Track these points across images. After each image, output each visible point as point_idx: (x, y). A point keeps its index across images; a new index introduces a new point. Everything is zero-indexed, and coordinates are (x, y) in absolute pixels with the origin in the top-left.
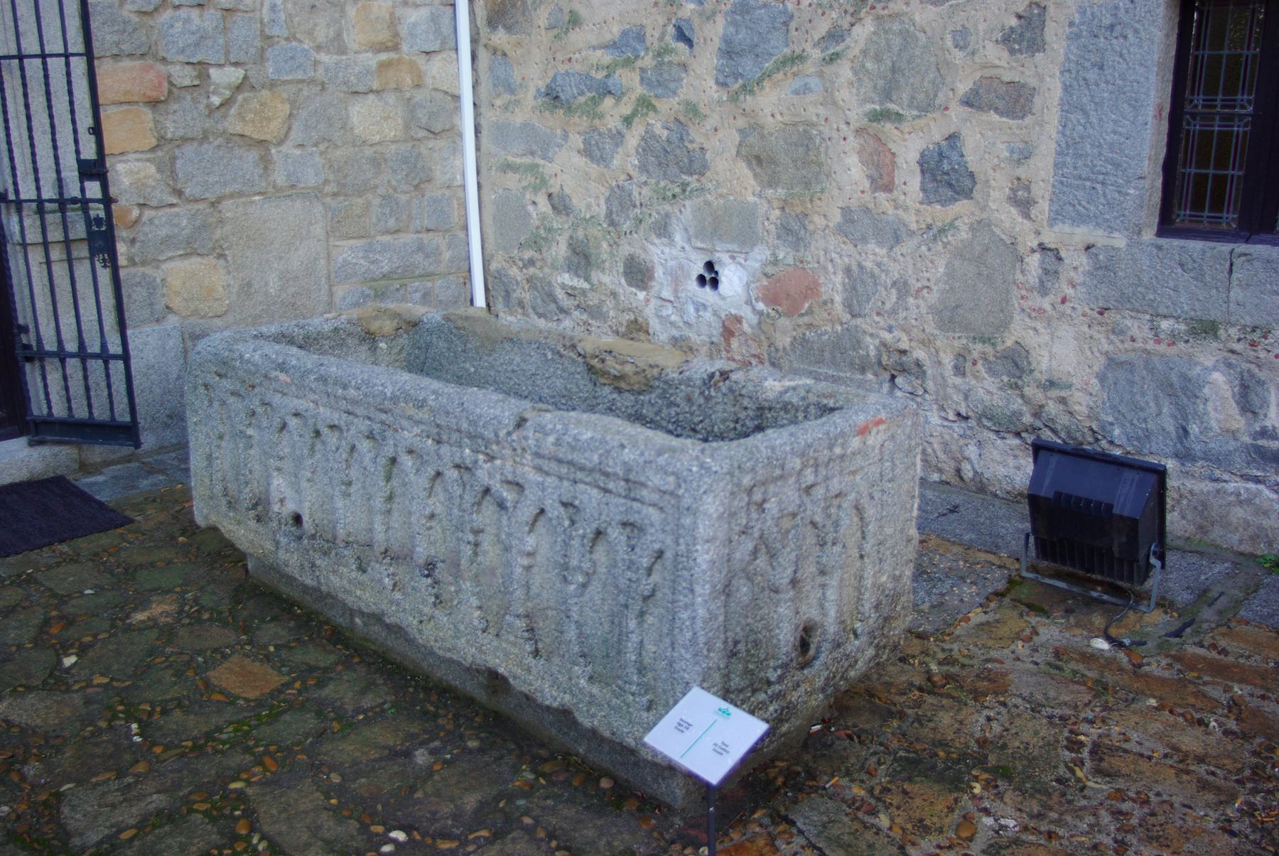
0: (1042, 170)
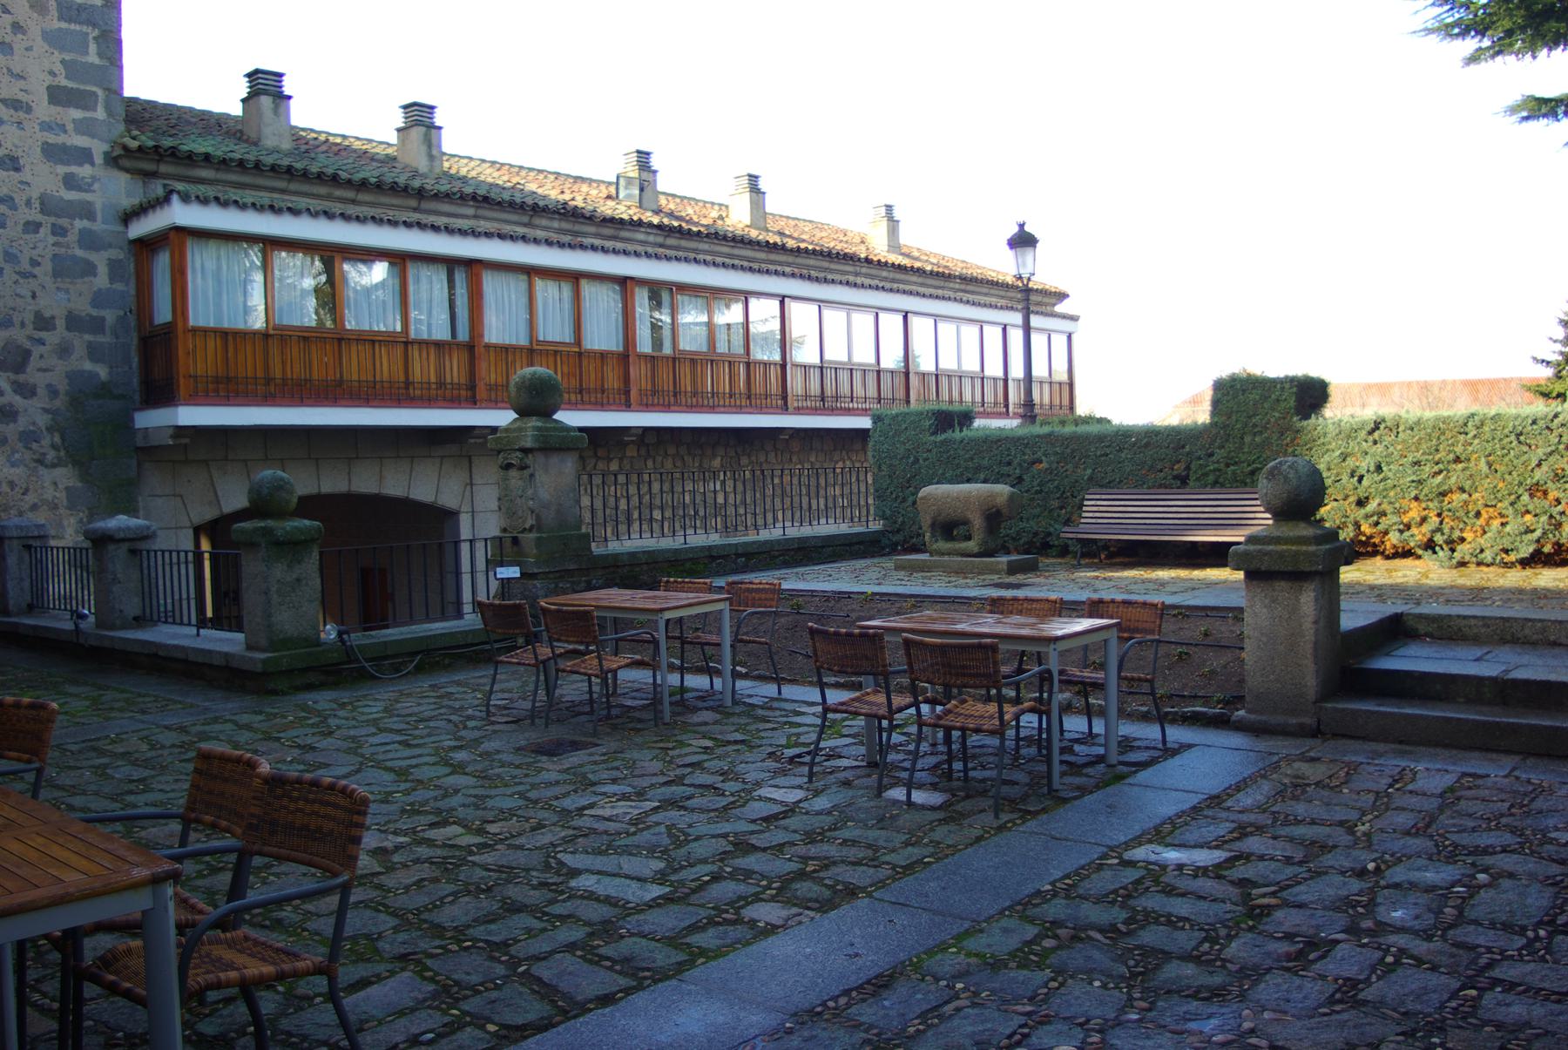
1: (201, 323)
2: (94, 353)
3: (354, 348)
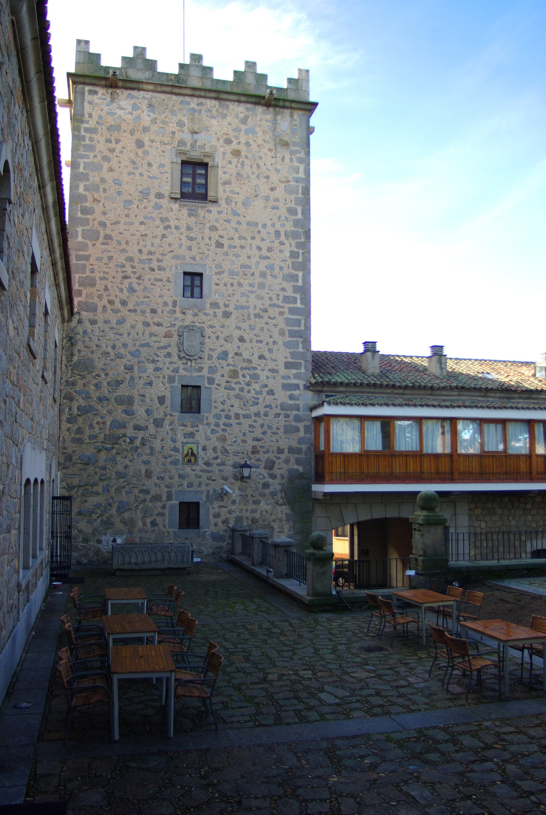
0: (167, 522)
1: (335, 451)
2: (298, 462)
3: (397, 459)
